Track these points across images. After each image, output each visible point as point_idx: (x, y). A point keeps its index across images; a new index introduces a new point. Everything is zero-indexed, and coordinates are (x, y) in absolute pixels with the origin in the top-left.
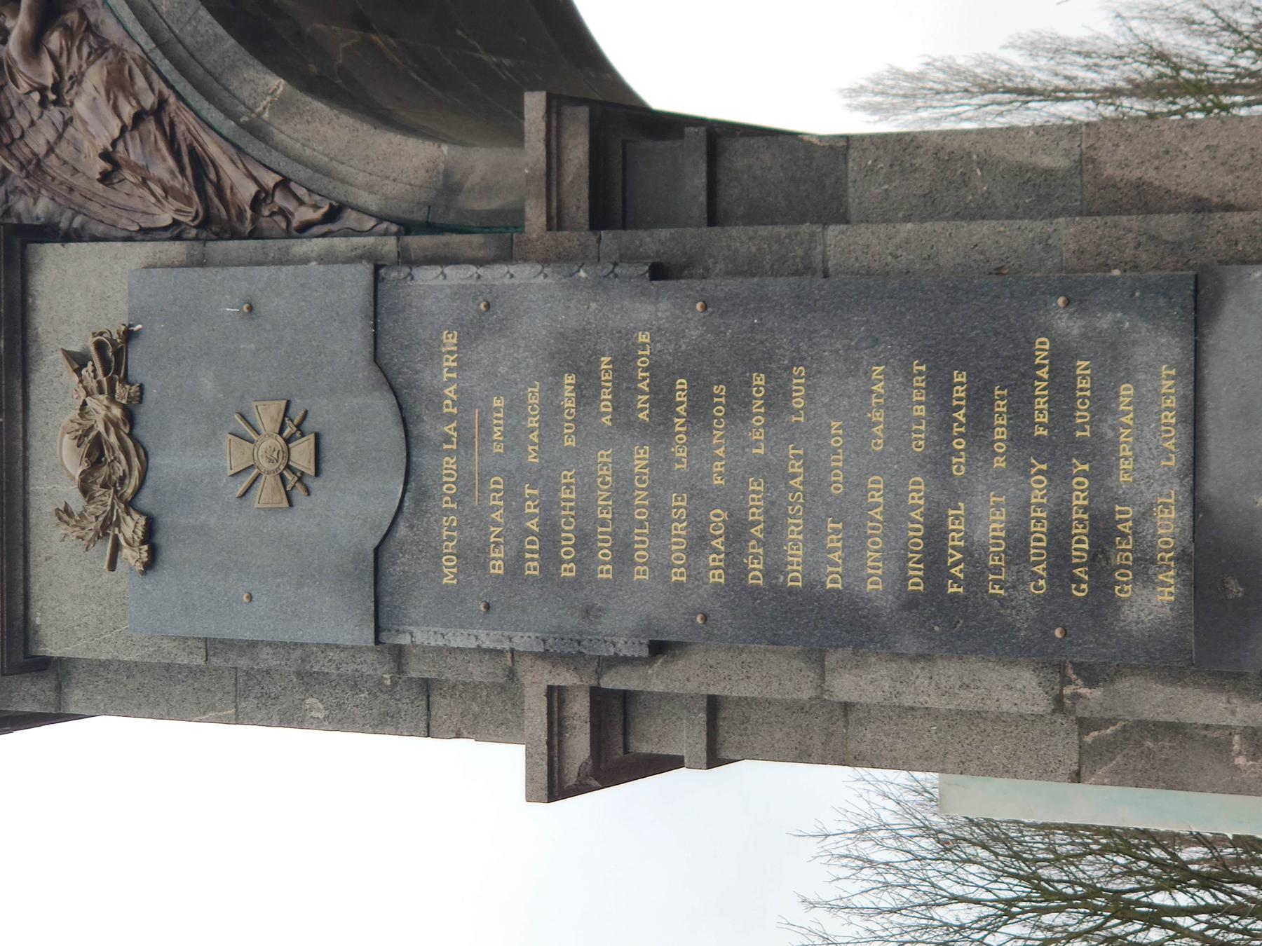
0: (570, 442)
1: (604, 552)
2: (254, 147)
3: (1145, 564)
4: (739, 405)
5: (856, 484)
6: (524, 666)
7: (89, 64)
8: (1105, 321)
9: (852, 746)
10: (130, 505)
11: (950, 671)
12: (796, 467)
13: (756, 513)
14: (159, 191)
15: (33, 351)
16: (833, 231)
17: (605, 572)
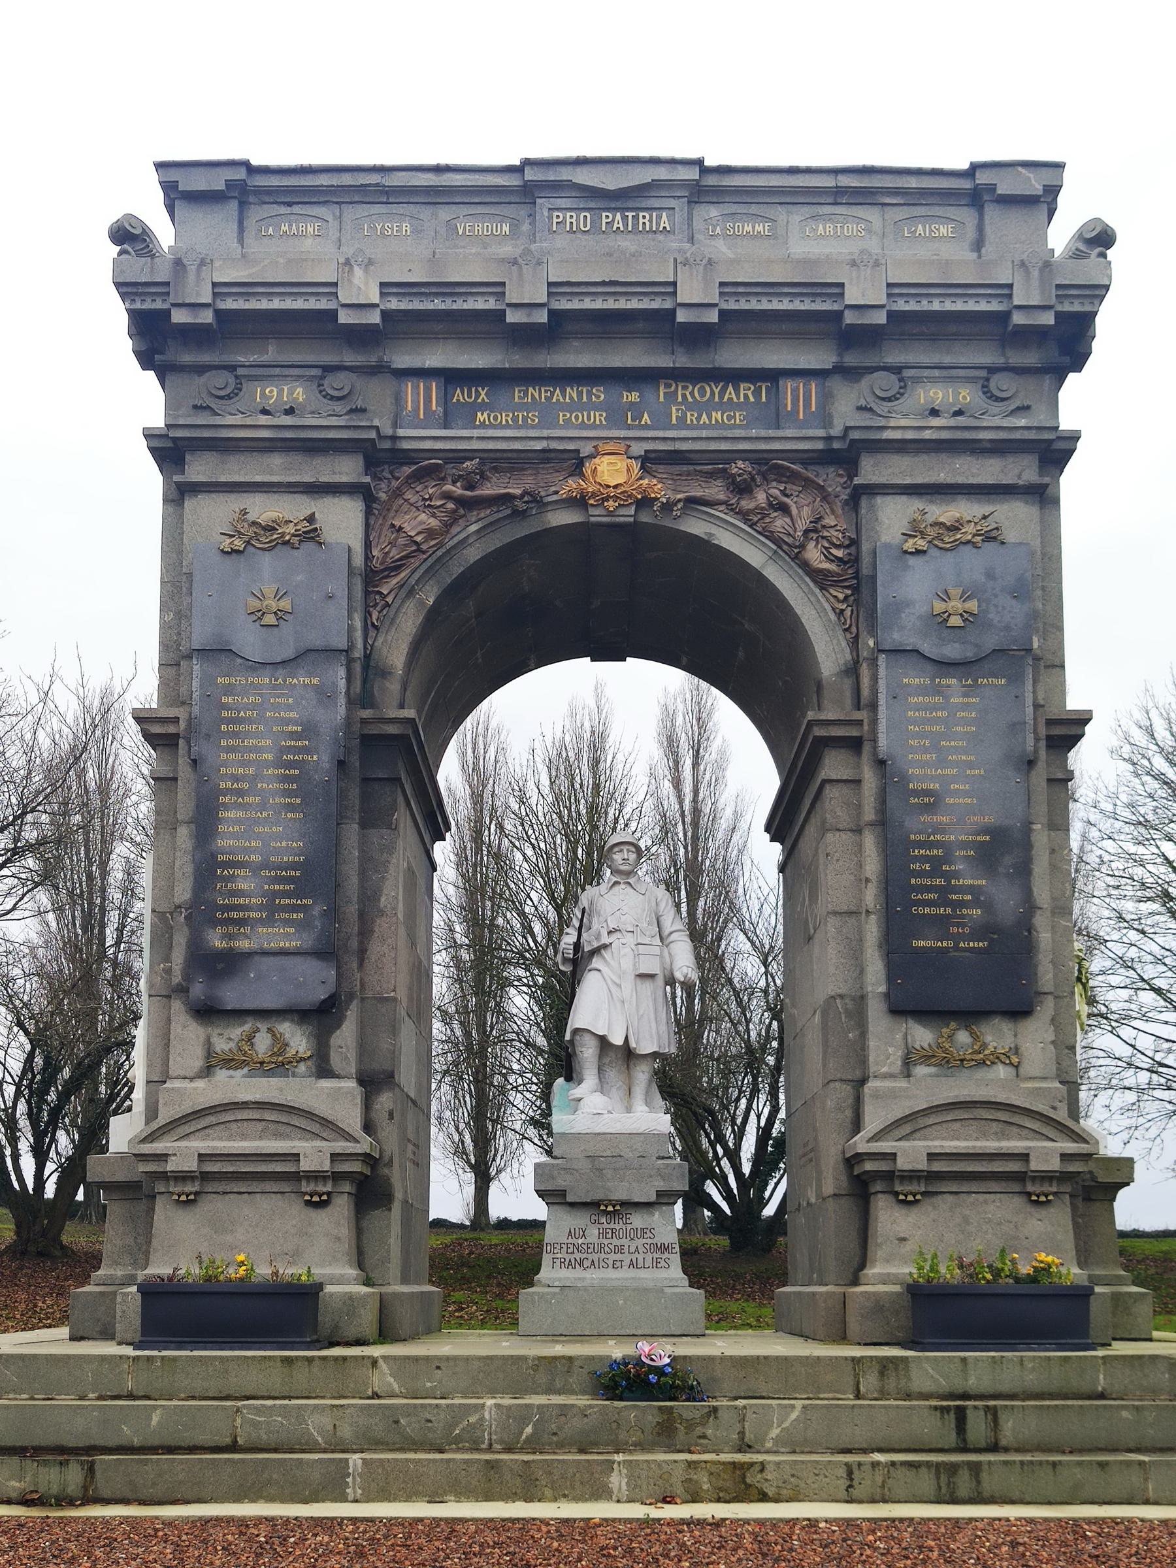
0: (275, 729)
1: (231, 742)
2: (403, 593)
3: (230, 937)
4: (288, 793)
5: (258, 836)
6: (187, 708)
7: (440, 521)
8: (318, 923)
9: (162, 831)
10: (248, 543)
11: (189, 869)
12: (265, 814)
13: (247, 800)
14: (387, 549)
15: (316, 496)
16: (356, 826)
17: (223, 742)
